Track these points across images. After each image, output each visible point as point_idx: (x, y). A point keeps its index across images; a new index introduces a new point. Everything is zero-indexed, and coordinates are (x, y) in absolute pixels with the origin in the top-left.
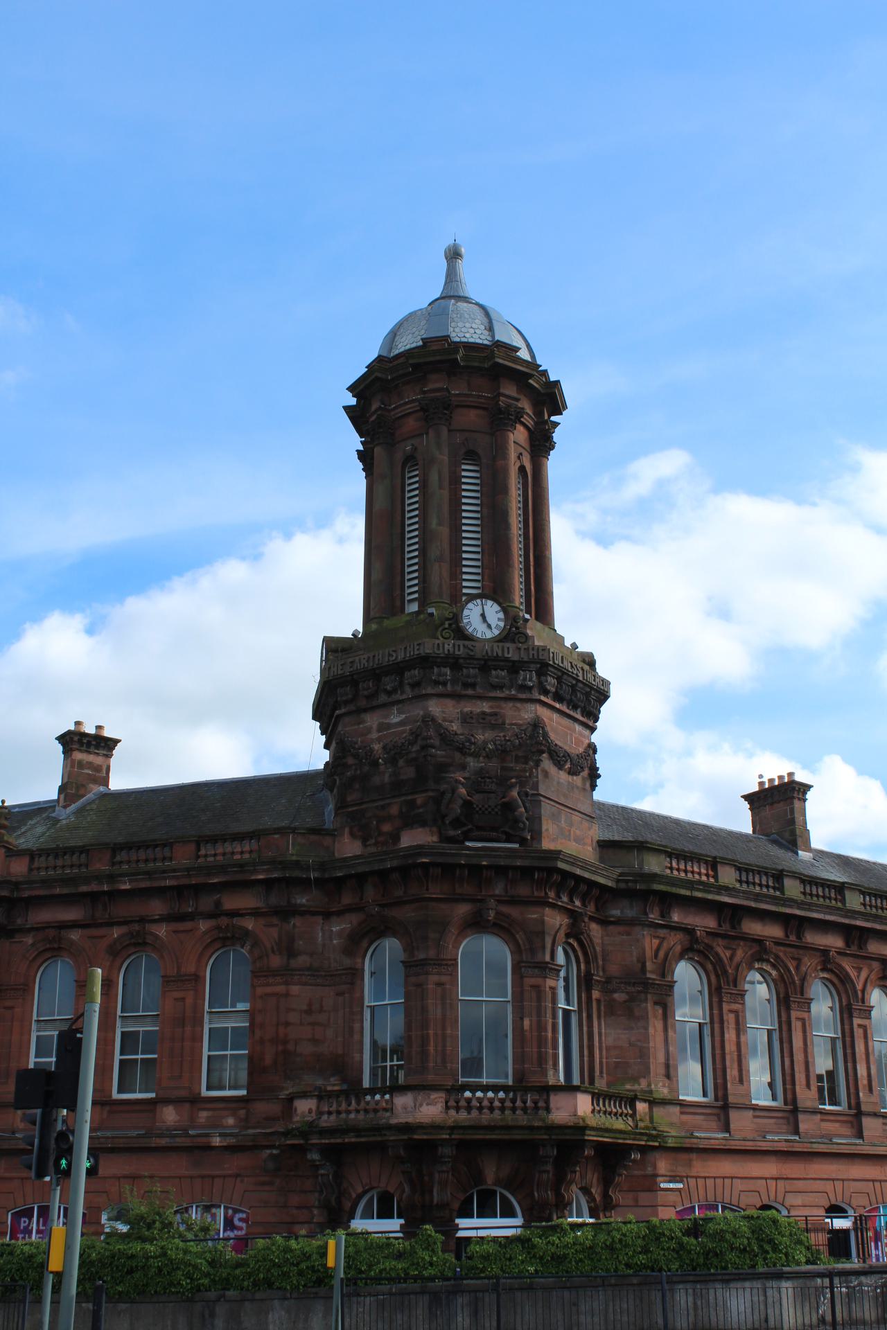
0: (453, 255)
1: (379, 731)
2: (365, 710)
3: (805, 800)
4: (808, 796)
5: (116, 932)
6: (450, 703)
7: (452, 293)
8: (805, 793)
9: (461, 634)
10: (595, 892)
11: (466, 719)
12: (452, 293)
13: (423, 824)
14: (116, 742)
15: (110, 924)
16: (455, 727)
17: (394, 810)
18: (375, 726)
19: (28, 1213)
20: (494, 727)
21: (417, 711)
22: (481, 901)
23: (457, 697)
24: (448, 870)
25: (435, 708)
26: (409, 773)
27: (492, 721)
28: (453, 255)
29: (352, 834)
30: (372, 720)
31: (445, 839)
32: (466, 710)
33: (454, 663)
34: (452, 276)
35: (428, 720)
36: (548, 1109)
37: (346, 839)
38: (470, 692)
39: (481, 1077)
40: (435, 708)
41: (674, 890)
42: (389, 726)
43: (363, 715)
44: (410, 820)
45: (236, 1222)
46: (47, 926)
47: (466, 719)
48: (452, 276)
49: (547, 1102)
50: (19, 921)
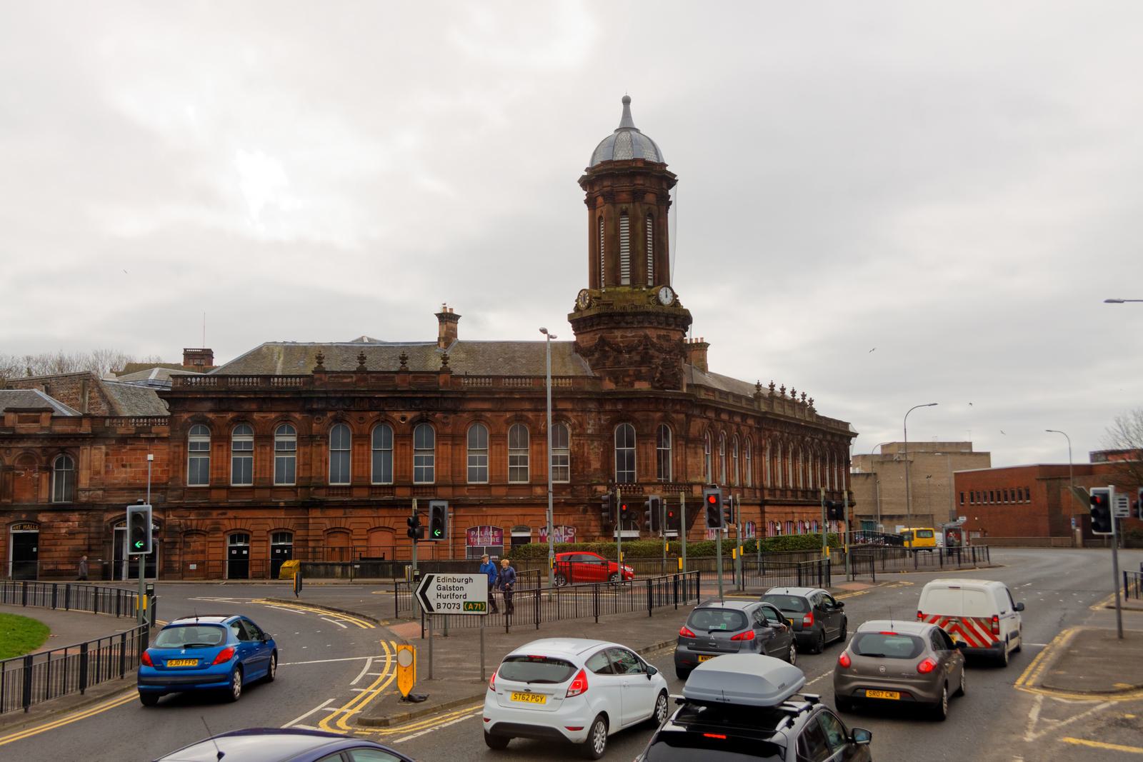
0: (626, 101)
1: (621, 338)
2: (615, 328)
3: (457, 323)
4: (459, 321)
5: (508, 415)
6: (653, 330)
7: (627, 126)
8: (457, 320)
9: (659, 303)
10: (130, 370)
11: (659, 337)
12: (627, 126)
13: (645, 380)
14: (437, 315)
15: (506, 411)
16: (655, 340)
17: (631, 373)
18: (619, 336)
19: (475, 529)
20: (667, 341)
21: (641, 333)
22: (666, 412)
23: (656, 328)
24: (657, 400)
25: (648, 332)
26: (637, 358)
27: (667, 338)
28: (626, 101)
29: (610, 380)
30: (618, 333)
31: (654, 387)
32: (659, 333)
33: (657, 315)
34: (627, 114)
35: (646, 337)
36: (692, 492)
37: (607, 381)
38: (660, 326)
39: (126, 531)
40: (648, 332)
41: (778, 418)
42: (627, 337)
43: (613, 330)
44: (639, 377)
45: (569, 532)
46: (474, 411)
47: (659, 337)
48: (627, 114)
49: (692, 489)
50: (461, 407)
